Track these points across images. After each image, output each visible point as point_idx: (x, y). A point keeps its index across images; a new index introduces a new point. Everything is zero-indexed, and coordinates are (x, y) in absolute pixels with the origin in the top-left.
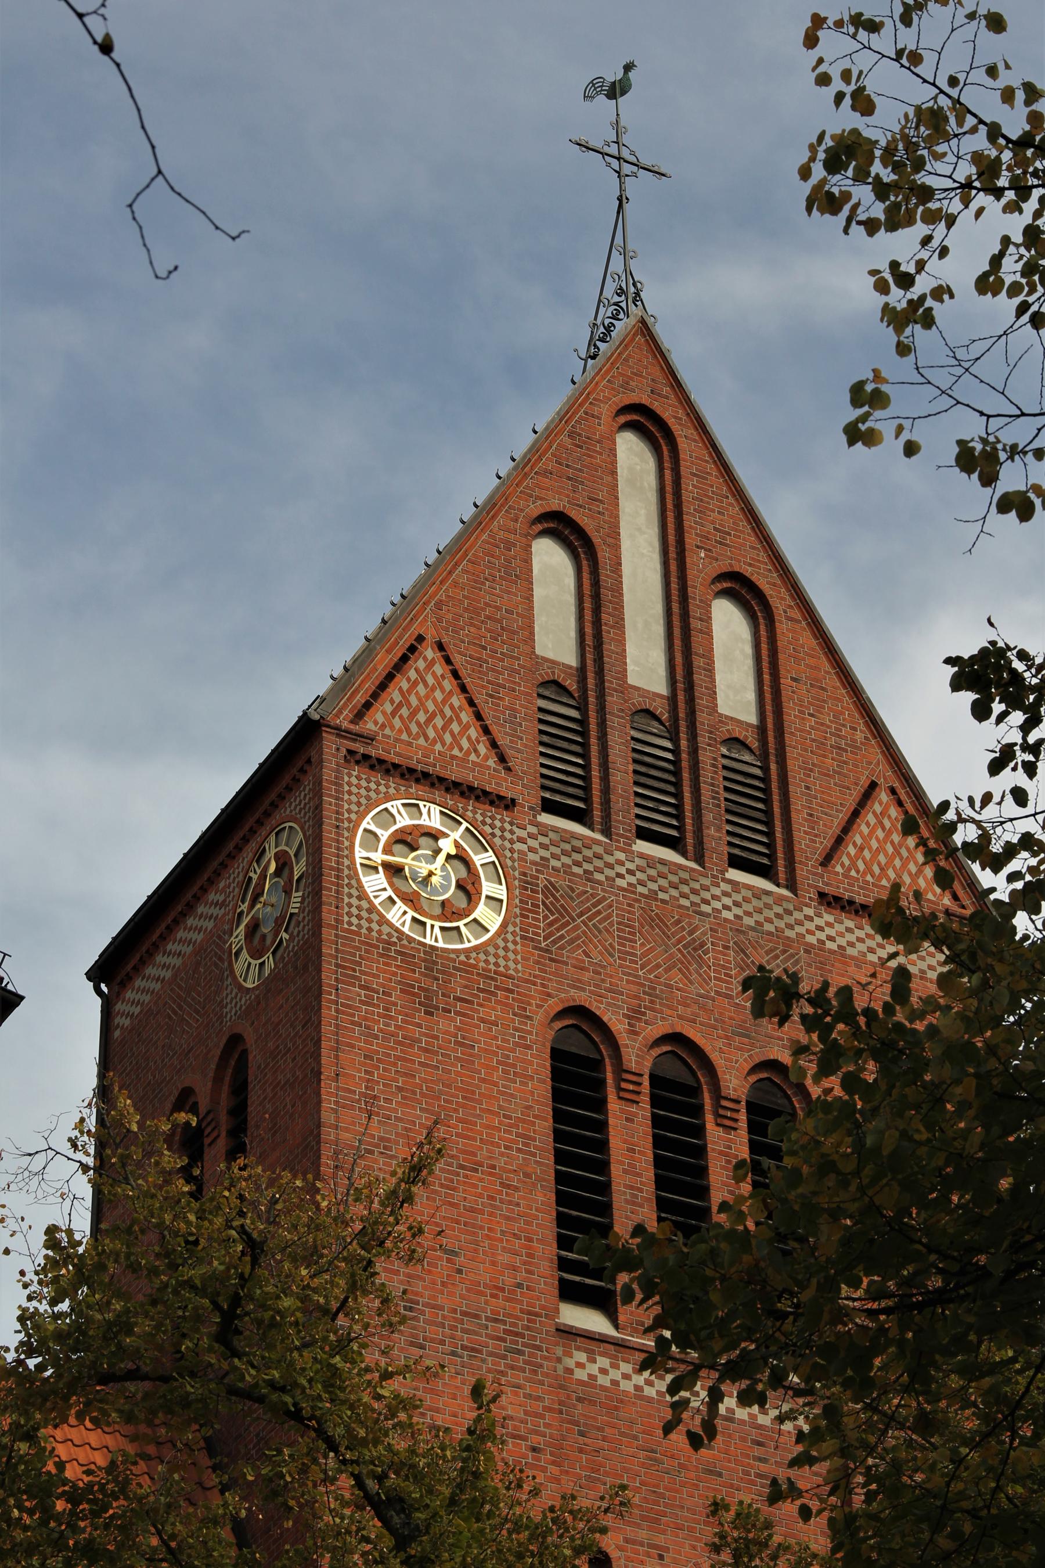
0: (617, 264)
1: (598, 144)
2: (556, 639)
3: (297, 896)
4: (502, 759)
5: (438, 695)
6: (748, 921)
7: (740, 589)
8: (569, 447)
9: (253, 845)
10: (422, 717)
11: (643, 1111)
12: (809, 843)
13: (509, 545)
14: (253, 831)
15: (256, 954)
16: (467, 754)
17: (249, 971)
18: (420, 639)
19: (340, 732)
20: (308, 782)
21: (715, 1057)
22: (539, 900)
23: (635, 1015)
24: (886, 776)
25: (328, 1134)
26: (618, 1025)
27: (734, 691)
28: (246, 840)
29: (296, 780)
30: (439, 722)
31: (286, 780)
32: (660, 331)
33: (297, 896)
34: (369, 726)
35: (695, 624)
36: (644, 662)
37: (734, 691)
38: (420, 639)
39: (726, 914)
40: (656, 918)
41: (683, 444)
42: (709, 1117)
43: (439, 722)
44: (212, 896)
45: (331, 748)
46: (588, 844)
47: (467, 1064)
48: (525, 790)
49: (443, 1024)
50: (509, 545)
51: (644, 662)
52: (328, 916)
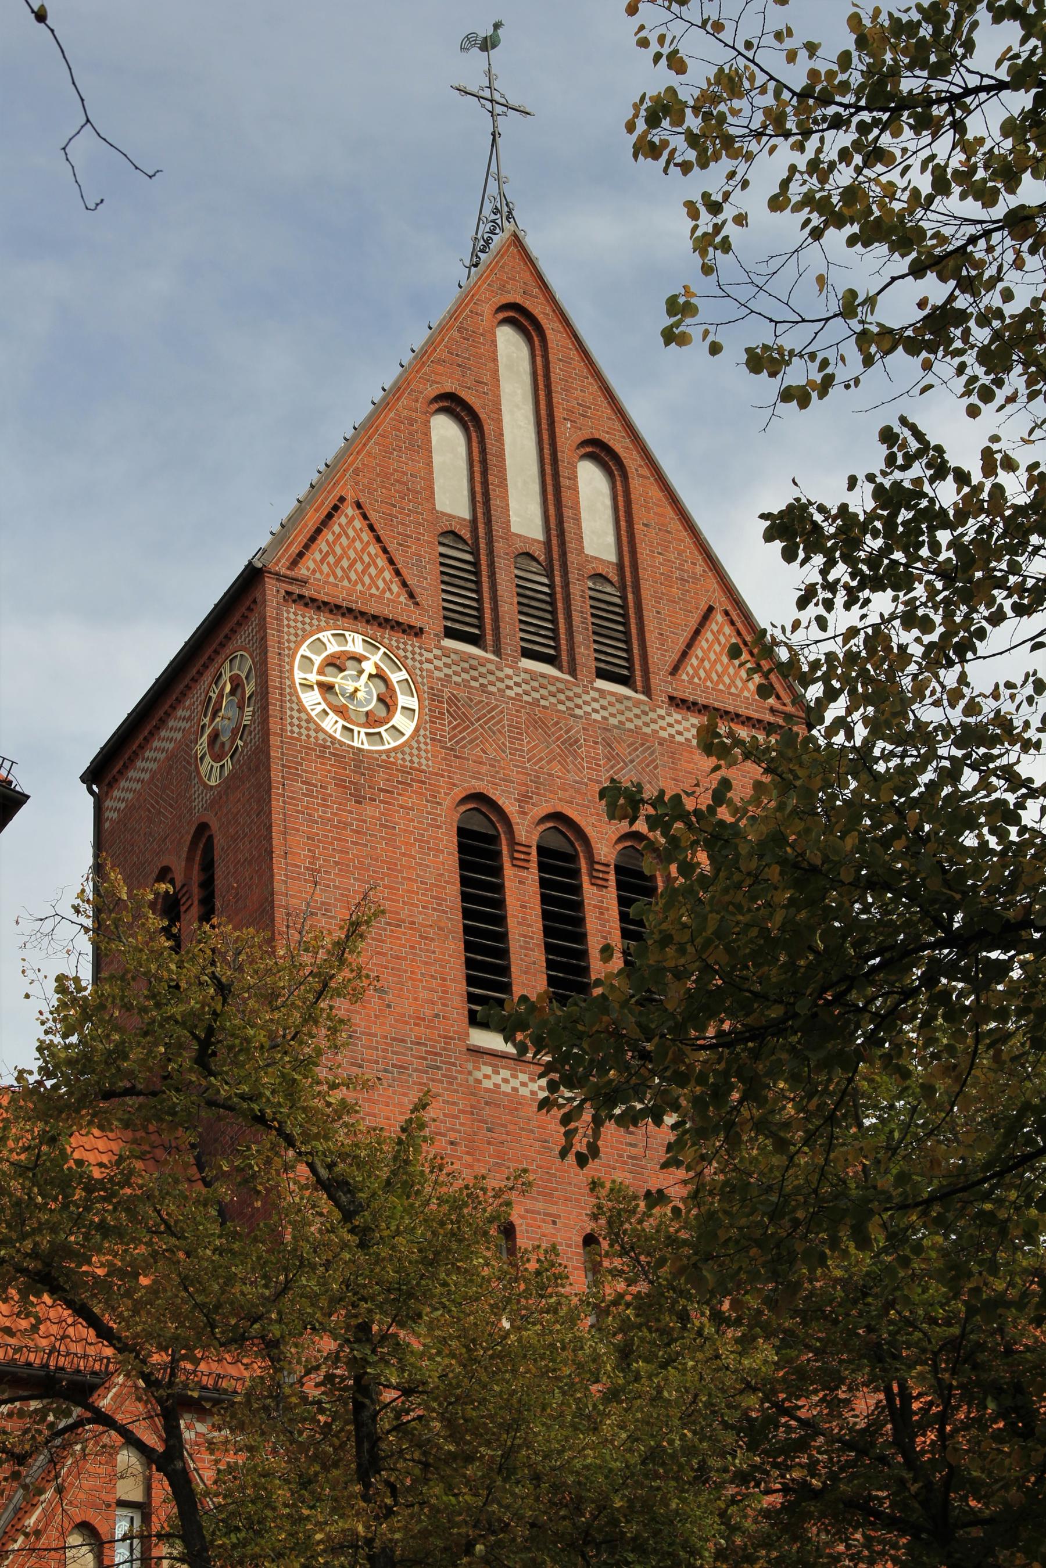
0: (493, 188)
2: (452, 497)
4: (411, 596)
5: (358, 545)
6: (613, 721)
9: (212, 670)
11: (532, 876)
12: (660, 657)
13: (411, 421)
14: (211, 659)
17: (212, 772)
18: (342, 499)
20: (254, 619)
22: (443, 708)
23: (524, 799)
24: (721, 602)
25: (280, 900)
27: (597, 536)
28: (206, 666)
29: (245, 617)
30: (359, 567)
31: (236, 617)
34: (302, 571)
36: (524, 515)
37: (597, 536)
40: (539, 722)
41: (550, 335)
42: (585, 879)
43: (359, 567)
44: (180, 713)
45: (272, 590)
47: (390, 842)
48: (432, 621)
49: (370, 811)
51: (524, 515)
52: (274, 726)
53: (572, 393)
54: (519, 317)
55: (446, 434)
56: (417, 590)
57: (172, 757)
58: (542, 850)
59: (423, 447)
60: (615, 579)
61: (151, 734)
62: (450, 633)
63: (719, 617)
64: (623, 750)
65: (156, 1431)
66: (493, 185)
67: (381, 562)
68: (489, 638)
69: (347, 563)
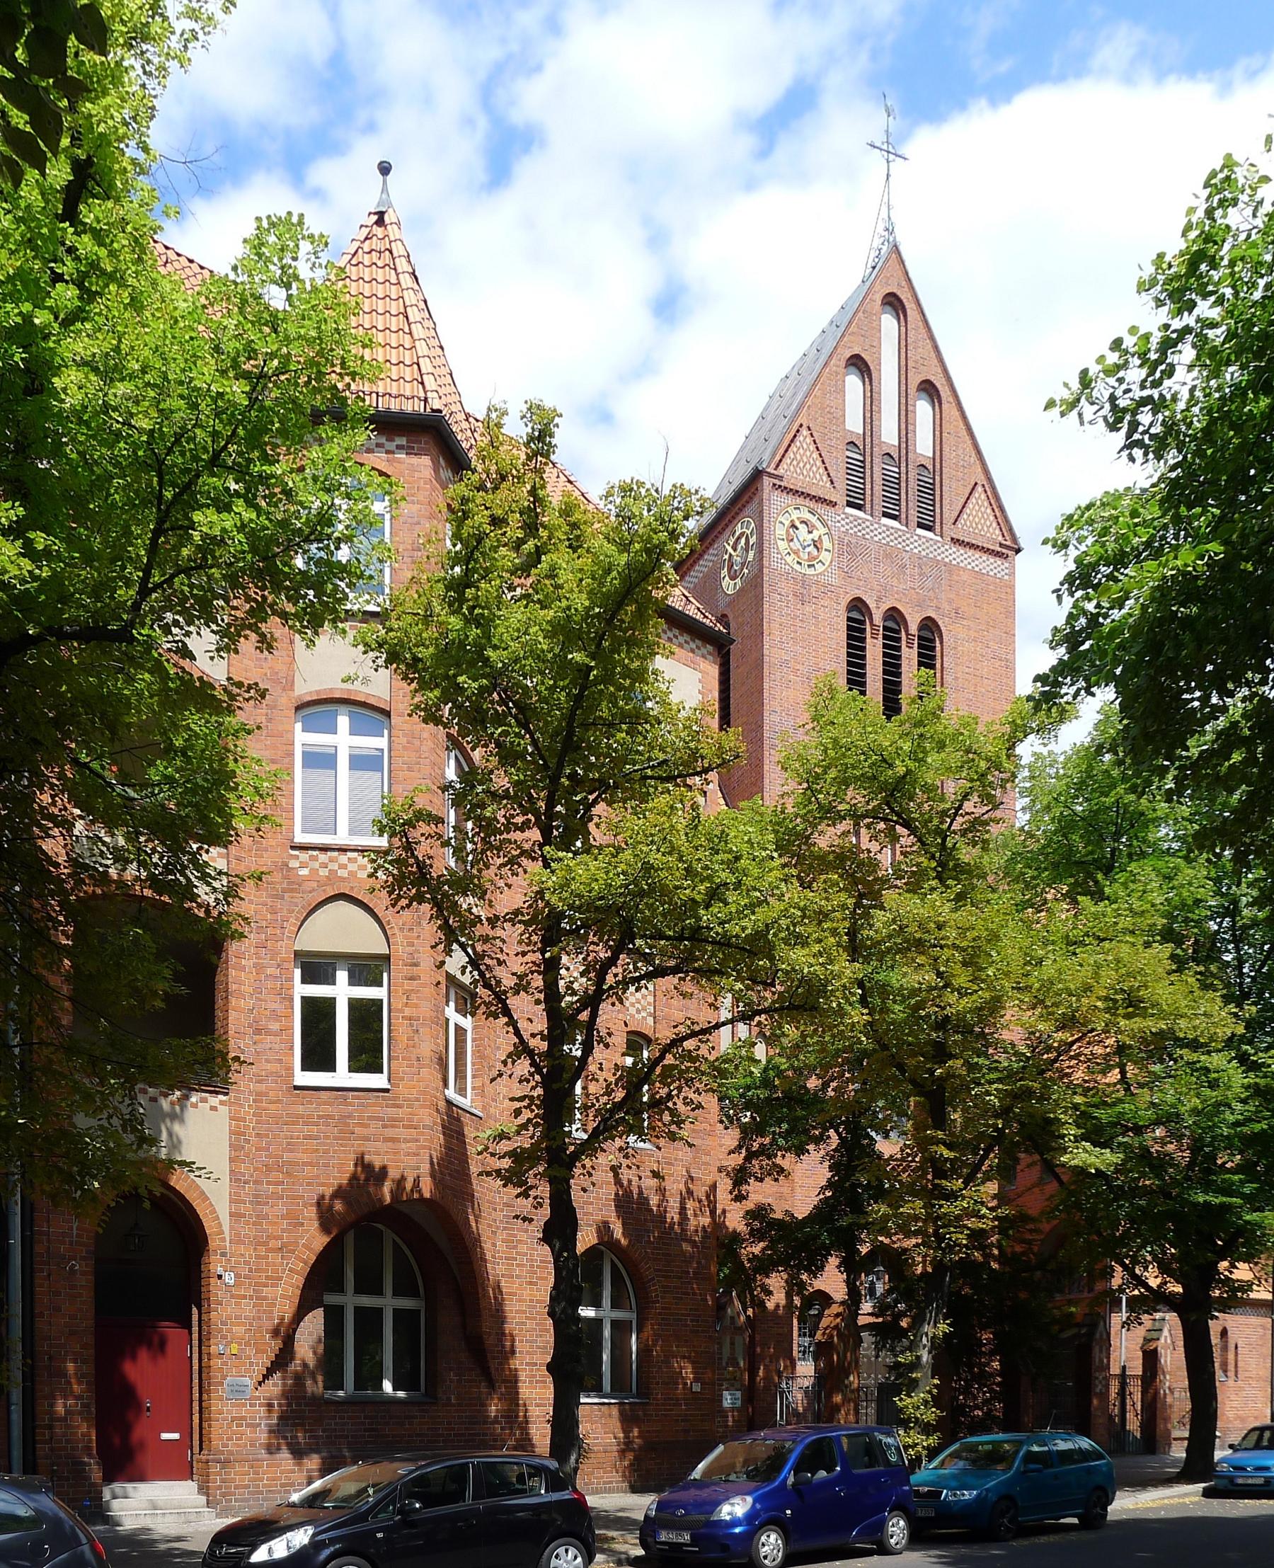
0: (884, 214)
1: (898, 159)
2: (854, 423)
3: (751, 554)
4: (832, 482)
5: (808, 453)
6: (923, 553)
7: (928, 389)
8: (855, 319)
9: (730, 528)
10: (801, 465)
11: (880, 641)
12: (949, 515)
13: (837, 374)
14: (730, 522)
15: (732, 578)
16: (815, 480)
17: (729, 586)
18: (801, 426)
19: (770, 475)
20: (756, 500)
21: (907, 616)
22: (849, 549)
23: (879, 600)
24: (981, 479)
25: (766, 659)
26: (872, 605)
27: (924, 445)
28: (727, 525)
29: (751, 498)
30: (808, 466)
31: (746, 498)
32: (901, 248)
33: (751, 554)
34: (781, 471)
35: (910, 408)
36: (889, 433)
37: (924, 445)
38: (801, 426)
39: (916, 551)
40: (889, 554)
41: (909, 312)
42: (904, 643)
43: (808, 466)
44: (711, 551)
45: (767, 481)
46: (865, 520)
47: (816, 625)
48: (841, 498)
49: (808, 609)
50: (837, 374)
51: (889, 433)
52: (766, 563)
53: (920, 351)
54: (894, 303)
55: (853, 383)
56: (835, 480)
57: (706, 576)
58: (885, 628)
59: (1138, 1528)
60: (931, 468)
61: (695, 562)
62: (850, 504)
63: (980, 489)
64: (926, 570)
65: (315, 1353)
66: (885, 209)
67: (819, 463)
68: (868, 506)
69: (802, 467)
